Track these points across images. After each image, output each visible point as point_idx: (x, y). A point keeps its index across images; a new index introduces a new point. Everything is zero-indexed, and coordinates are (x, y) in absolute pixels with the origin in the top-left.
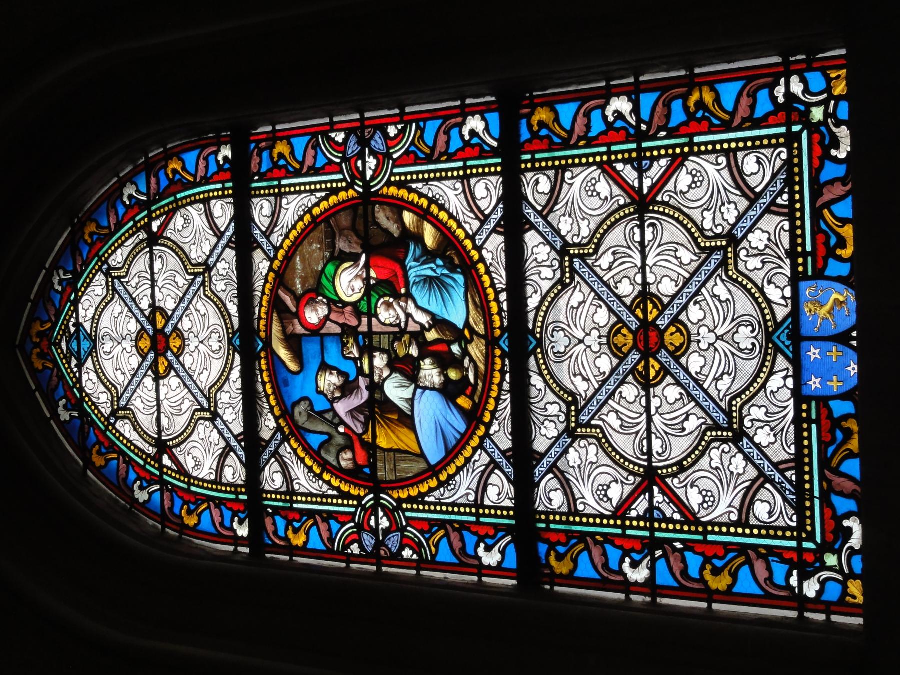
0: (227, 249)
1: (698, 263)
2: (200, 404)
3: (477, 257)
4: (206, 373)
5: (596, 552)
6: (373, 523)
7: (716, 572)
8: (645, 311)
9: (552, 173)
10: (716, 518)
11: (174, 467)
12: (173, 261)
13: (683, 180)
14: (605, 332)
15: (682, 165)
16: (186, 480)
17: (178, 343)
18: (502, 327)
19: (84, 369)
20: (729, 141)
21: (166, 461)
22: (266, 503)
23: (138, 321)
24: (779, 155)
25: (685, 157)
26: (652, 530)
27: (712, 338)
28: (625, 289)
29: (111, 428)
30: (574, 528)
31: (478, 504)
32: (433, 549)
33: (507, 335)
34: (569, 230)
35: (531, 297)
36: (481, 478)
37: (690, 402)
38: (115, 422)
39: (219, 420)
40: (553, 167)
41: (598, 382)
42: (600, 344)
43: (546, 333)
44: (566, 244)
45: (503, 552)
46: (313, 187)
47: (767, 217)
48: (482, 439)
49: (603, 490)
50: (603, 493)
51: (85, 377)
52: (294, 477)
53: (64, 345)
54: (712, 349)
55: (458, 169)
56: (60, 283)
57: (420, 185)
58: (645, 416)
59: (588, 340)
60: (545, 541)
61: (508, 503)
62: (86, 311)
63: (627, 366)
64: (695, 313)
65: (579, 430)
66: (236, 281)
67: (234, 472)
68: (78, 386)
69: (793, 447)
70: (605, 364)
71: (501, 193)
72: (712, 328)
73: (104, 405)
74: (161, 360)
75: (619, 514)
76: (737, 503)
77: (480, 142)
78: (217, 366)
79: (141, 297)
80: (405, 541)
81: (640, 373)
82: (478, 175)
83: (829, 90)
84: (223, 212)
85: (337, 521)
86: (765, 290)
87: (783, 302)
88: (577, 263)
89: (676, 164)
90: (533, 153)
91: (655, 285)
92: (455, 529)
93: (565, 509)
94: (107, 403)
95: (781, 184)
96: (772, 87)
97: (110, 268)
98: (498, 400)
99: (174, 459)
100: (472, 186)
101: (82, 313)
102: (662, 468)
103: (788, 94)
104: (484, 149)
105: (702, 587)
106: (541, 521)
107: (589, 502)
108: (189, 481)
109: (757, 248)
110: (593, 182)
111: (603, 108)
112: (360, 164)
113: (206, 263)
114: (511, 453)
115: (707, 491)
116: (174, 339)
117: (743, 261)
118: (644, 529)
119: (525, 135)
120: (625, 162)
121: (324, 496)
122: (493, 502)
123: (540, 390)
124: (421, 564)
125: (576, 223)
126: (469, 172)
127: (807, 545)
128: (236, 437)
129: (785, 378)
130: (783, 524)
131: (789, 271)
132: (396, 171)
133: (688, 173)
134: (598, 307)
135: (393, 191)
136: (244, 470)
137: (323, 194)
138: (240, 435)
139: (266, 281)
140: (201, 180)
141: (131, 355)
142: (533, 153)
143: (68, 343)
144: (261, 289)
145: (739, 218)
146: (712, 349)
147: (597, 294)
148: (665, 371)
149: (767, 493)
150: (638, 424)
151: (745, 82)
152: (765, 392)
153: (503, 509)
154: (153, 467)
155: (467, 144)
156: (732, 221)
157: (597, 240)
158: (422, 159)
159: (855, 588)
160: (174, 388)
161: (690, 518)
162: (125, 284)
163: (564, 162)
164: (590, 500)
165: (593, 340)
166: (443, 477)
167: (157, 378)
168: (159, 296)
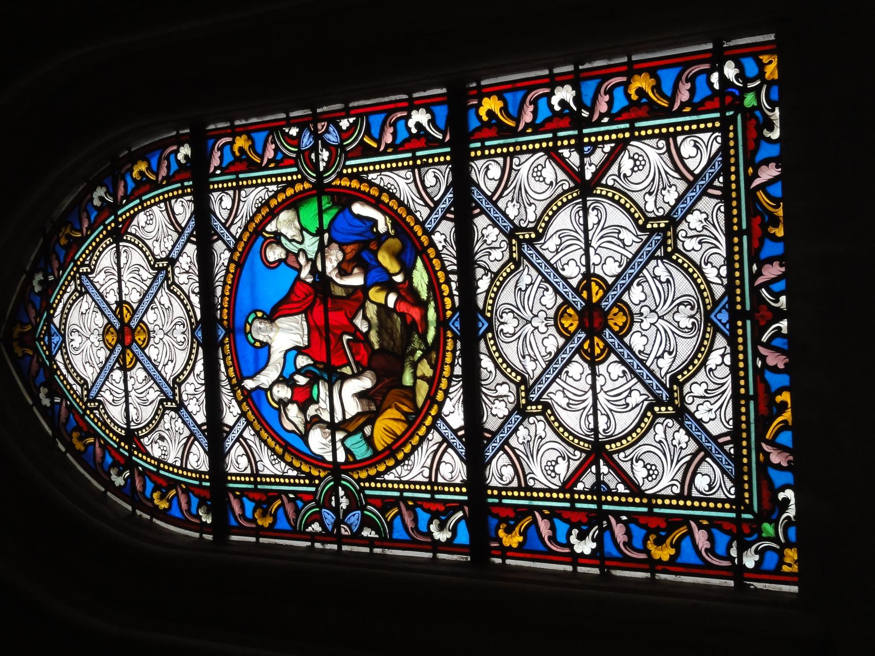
2: (165, 395)
3: (426, 244)
4: (171, 365)
6: (333, 503)
10: (660, 491)
12: (137, 257)
13: (626, 163)
14: (551, 313)
17: (621, 320)
18: (453, 309)
20: (667, 126)
22: (231, 485)
24: (716, 138)
26: (599, 503)
35: (481, 278)
39: (183, 410)
42: (546, 325)
47: (444, 222)
49: (552, 465)
50: (550, 469)
54: (654, 328)
58: (590, 392)
59: (535, 322)
60: (496, 516)
65: (529, 408)
66: (197, 273)
67: (199, 459)
69: (731, 422)
70: (553, 343)
75: (567, 487)
76: (679, 477)
78: (181, 357)
80: (295, 142)
81: (586, 351)
82: (683, 132)
83: (761, 75)
84: (184, 209)
85: (302, 501)
90: (482, 141)
91: (600, 266)
92: (544, 517)
93: (248, 471)
95: (719, 165)
96: (709, 73)
100: (679, 143)
102: (138, 430)
103: (723, 79)
105: (567, 550)
106: (492, 496)
107: (539, 477)
109: (695, 229)
110: (650, 478)
111: (626, 85)
112: (313, 156)
113: (167, 259)
115: (652, 465)
116: (139, 332)
117: (681, 241)
118: (592, 502)
119: (474, 124)
120: (569, 146)
123: (490, 372)
124: (386, 541)
126: (419, 162)
127: (745, 516)
128: (455, 432)
130: (723, 496)
131: (725, 252)
132: (348, 163)
133: (559, 475)
139: (228, 271)
142: (482, 141)
144: (222, 279)
147: (544, 276)
148: (609, 349)
149: (489, 186)
150: (584, 401)
151: (525, 91)
159: (791, 555)
160: (614, 377)
161: (635, 489)
163: (671, 130)
164: (540, 476)
167: (124, 369)
168: (125, 290)
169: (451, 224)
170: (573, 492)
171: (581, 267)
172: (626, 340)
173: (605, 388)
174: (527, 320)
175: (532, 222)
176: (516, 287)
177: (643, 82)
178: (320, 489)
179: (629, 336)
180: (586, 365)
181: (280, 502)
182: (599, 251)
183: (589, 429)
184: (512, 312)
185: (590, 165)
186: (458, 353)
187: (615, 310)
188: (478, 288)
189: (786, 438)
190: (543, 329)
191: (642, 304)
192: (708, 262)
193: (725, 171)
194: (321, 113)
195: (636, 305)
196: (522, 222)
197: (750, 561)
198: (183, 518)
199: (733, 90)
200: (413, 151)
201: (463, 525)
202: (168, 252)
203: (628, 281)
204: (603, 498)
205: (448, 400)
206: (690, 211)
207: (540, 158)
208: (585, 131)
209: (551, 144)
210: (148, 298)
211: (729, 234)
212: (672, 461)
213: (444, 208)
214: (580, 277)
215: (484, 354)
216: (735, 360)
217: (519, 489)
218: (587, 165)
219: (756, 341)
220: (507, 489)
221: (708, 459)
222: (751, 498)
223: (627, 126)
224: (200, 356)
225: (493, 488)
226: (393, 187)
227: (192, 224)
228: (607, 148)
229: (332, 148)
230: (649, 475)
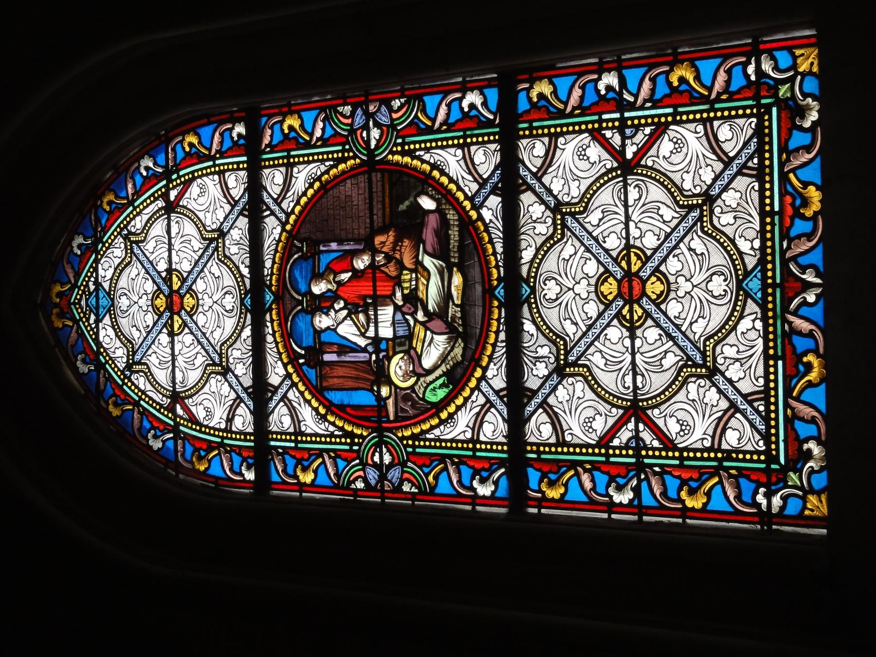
1: (588, 353)
8: (629, 263)
10: (691, 444)
11: (186, 416)
12: (189, 228)
13: (665, 146)
14: (672, 295)
15: (664, 132)
17: (158, 302)
18: (499, 279)
21: (180, 411)
22: (273, 443)
23: (154, 282)
25: (667, 125)
27: (688, 286)
28: (613, 243)
29: (126, 381)
31: (290, 166)
33: (503, 284)
35: (526, 249)
38: (131, 375)
44: (559, 204)
46: (445, 143)
47: (739, 177)
48: (479, 380)
51: (102, 333)
52: (301, 419)
53: (83, 303)
54: (211, 310)
55: (458, 138)
59: (688, 286)
61: (502, 439)
62: (105, 272)
67: (244, 420)
70: (673, 265)
72: (688, 277)
73: (119, 359)
74: (176, 317)
76: (710, 431)
77: (688, 88)
78: (230, 324)
79: (605, 234)
82: (477, 143)
84: (237, 183)
85: (345, 460)
87: (106, 327)
88: (569, 220)
89: (660, 130)
92: (453, 463)
93: (292, 430)
94: (122, 357)
96: (745, 65)
97: (130, 233)
98: (494, 346)
99: (186, 409)
101: (101, 272)
102: (182, 392)
103: (759, 71)
106: (532, 452)
109: (730, 206)
114: (505, 392)
115: (683, 421)
119: (523, 105)
121: (332, 435)
122: (731, 446)
127: (773, 466)
129: (754, 321)
133: (596, 431)
136: (506, 425)
138: (249, 387)
146: (211, 310)
149: (737, 421)
153: (498, 444)
155: (465, 115)
156: (709, 182)
157: (586, 198)
161: (668, 443)
162: (581, 220)
164: (690, 137)
166: (444, 415)
167: (171, 334)
168: (175, 259)
169: (246, 220)
170: (608, 447)
171: (622, 239)
172: (663, 307)
173: (641, 350)
178: (363, 447)
179: (196, 315)
180: (624, 330)
181: (217, 452)
182: (640, 225)
185: (633, 144)
186: (502, 320)
188: (522, 258)
189: (818, 396)
191: (678, 274)
192: (742, 236)
193: (760, 151)
195: (672, 275)
196: (702, 385)
198: (455, 493)
199: (767, 80)
200: (464, 130)
201: (504, 479)
202: (219, 224)
205: (492, 364)
206: (725, 189)
209: (340, 155)
211: (763, 214)
212: (704, 416)
213: (740, 164)
215: (526, 319)
216: (766, 326)
217: (556, 445)
218: (629, 145)
220: (545, 445)
223: (462, 133)
224: (249, 321)
225: (532, 444)
226: (442, 164)
228: (648, 130)
229: (385, 128)
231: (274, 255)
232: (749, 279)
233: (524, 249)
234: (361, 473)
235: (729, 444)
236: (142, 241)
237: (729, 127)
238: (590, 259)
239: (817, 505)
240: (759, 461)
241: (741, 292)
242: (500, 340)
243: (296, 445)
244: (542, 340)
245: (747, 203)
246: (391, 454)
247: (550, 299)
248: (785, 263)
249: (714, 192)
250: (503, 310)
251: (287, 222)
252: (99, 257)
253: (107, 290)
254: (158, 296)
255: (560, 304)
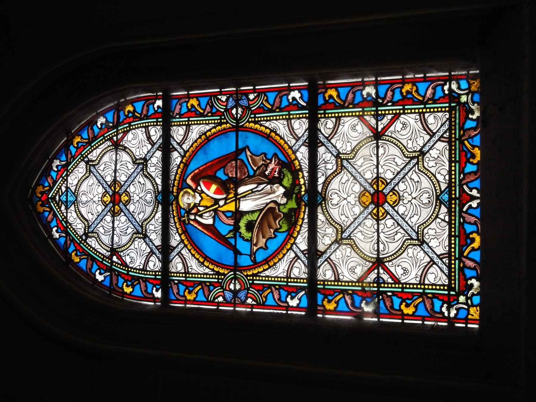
0: (157, 151)
1: (97, 227)
5: (143, 285)
7: (408, 306)
8: (115, 188)
9: (334, 120)
13: (398, 125)
14: (401, 203)
15: (398, 118)
16: (126, 269)
17: (126, 198)
18: (172, 204)
19: (69, 211)
21: (115, 259)
25: (400, 114)
27: (349, 199)
29: (83, 242)
30: (147, 276)
32: (264, 299)
34: (341, 147)
35: (321, 177)
36: (146, 258)
37: (398, 226)
40: (335, 117)
41: (135, 181)
43: (79, 196)
44: (144, 239)
45: (300, 299)
47: (439, 142)
48: (185, 156)
49: (353, 269)
56: (57, 167)
57: (264, 122)
62: (73, 180)
63: (108, 209)
64: (402, 186)
67: (155, 264)
68: (65, 220)
70: (132, 189)
71: (307, 127)
72: (410, 193)
77: (334, 101)
78: (149, 210)
79: (393, 227)
81: (375, 214)
84: (156, 133)
86: (436, 176)
87: (72, 211)
92: (276, 289)
93: (183, 271)
96: (443, 85)
99: (120, 257)
103: (450, 89)
104: (336, 105)
105: (400, 313)
106: (320, 284)
107: (346, 275)
108: (128, 269)
119: (321, 101)
122: (296, 276)
125: (140, 247)
126: (190, 123)
127: (452, 293)
133: (357, 274)
134: (355, 183)
135: (252, 125)
137: (213, 125)
140: (144, 117)
141: (97, 205)
143: (60, 196)
145: (148, 152)
149: (434, 269)
152: (436, 221)
154: (108, 262)
158: (338, 106)
161: (396, 281)
164: (346, 273)
165: (352, 199)
170: (363, 283)
174: (141, 199)
175: (349, 151)
176: (340, 181)
177: (194, 102)
179: (129, 206)
180: (374, 221)
183: (375, 251)
184: (337, 193)
187: (391, 193)
189: (476, 255)
190: (406, 195)
191: (404, 191)
194: (454, 75)
197: (453, 313)
198: (276, 304)
201: (305, 297)
203: (129, 183)
204: (220, 277)
207: (355, 120)
208: (379, 108)
210: (131, 179)
211: (450, 161)
214: (112, 181)
217: (334, 281)
219: (461, 211)
221: (154, 255)
222: (455, 284)
227: (161, 141)
228: (390, 117)
230: (131, 261)
231: (302, 223)
232: (443, 194)
233: (319, 177)
234: (222, 294)
235: (429, 281)
236: (97, 165)
237: (433, 117)
238: (356, 184)
239: (475, 313)
240: (444, 290)
241: (439, 201)
242: (174, 176)
243: (186, 279)
244: (153, 174)
245: (443, 156)
246: (240, 284)
247: (149, 193)
248: (461, 186)
249: (426, 149)
250: (307, 208)
251: (292, 245)
252: (69, 173)
253: (73, 191)
254: (105, 196)
255: (145, 191)
